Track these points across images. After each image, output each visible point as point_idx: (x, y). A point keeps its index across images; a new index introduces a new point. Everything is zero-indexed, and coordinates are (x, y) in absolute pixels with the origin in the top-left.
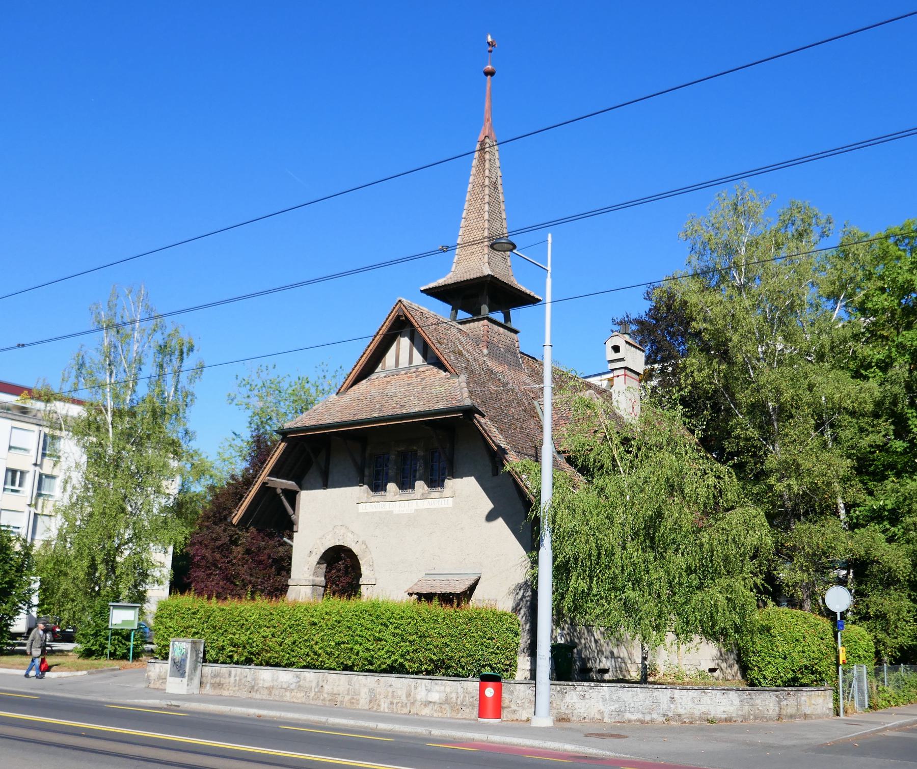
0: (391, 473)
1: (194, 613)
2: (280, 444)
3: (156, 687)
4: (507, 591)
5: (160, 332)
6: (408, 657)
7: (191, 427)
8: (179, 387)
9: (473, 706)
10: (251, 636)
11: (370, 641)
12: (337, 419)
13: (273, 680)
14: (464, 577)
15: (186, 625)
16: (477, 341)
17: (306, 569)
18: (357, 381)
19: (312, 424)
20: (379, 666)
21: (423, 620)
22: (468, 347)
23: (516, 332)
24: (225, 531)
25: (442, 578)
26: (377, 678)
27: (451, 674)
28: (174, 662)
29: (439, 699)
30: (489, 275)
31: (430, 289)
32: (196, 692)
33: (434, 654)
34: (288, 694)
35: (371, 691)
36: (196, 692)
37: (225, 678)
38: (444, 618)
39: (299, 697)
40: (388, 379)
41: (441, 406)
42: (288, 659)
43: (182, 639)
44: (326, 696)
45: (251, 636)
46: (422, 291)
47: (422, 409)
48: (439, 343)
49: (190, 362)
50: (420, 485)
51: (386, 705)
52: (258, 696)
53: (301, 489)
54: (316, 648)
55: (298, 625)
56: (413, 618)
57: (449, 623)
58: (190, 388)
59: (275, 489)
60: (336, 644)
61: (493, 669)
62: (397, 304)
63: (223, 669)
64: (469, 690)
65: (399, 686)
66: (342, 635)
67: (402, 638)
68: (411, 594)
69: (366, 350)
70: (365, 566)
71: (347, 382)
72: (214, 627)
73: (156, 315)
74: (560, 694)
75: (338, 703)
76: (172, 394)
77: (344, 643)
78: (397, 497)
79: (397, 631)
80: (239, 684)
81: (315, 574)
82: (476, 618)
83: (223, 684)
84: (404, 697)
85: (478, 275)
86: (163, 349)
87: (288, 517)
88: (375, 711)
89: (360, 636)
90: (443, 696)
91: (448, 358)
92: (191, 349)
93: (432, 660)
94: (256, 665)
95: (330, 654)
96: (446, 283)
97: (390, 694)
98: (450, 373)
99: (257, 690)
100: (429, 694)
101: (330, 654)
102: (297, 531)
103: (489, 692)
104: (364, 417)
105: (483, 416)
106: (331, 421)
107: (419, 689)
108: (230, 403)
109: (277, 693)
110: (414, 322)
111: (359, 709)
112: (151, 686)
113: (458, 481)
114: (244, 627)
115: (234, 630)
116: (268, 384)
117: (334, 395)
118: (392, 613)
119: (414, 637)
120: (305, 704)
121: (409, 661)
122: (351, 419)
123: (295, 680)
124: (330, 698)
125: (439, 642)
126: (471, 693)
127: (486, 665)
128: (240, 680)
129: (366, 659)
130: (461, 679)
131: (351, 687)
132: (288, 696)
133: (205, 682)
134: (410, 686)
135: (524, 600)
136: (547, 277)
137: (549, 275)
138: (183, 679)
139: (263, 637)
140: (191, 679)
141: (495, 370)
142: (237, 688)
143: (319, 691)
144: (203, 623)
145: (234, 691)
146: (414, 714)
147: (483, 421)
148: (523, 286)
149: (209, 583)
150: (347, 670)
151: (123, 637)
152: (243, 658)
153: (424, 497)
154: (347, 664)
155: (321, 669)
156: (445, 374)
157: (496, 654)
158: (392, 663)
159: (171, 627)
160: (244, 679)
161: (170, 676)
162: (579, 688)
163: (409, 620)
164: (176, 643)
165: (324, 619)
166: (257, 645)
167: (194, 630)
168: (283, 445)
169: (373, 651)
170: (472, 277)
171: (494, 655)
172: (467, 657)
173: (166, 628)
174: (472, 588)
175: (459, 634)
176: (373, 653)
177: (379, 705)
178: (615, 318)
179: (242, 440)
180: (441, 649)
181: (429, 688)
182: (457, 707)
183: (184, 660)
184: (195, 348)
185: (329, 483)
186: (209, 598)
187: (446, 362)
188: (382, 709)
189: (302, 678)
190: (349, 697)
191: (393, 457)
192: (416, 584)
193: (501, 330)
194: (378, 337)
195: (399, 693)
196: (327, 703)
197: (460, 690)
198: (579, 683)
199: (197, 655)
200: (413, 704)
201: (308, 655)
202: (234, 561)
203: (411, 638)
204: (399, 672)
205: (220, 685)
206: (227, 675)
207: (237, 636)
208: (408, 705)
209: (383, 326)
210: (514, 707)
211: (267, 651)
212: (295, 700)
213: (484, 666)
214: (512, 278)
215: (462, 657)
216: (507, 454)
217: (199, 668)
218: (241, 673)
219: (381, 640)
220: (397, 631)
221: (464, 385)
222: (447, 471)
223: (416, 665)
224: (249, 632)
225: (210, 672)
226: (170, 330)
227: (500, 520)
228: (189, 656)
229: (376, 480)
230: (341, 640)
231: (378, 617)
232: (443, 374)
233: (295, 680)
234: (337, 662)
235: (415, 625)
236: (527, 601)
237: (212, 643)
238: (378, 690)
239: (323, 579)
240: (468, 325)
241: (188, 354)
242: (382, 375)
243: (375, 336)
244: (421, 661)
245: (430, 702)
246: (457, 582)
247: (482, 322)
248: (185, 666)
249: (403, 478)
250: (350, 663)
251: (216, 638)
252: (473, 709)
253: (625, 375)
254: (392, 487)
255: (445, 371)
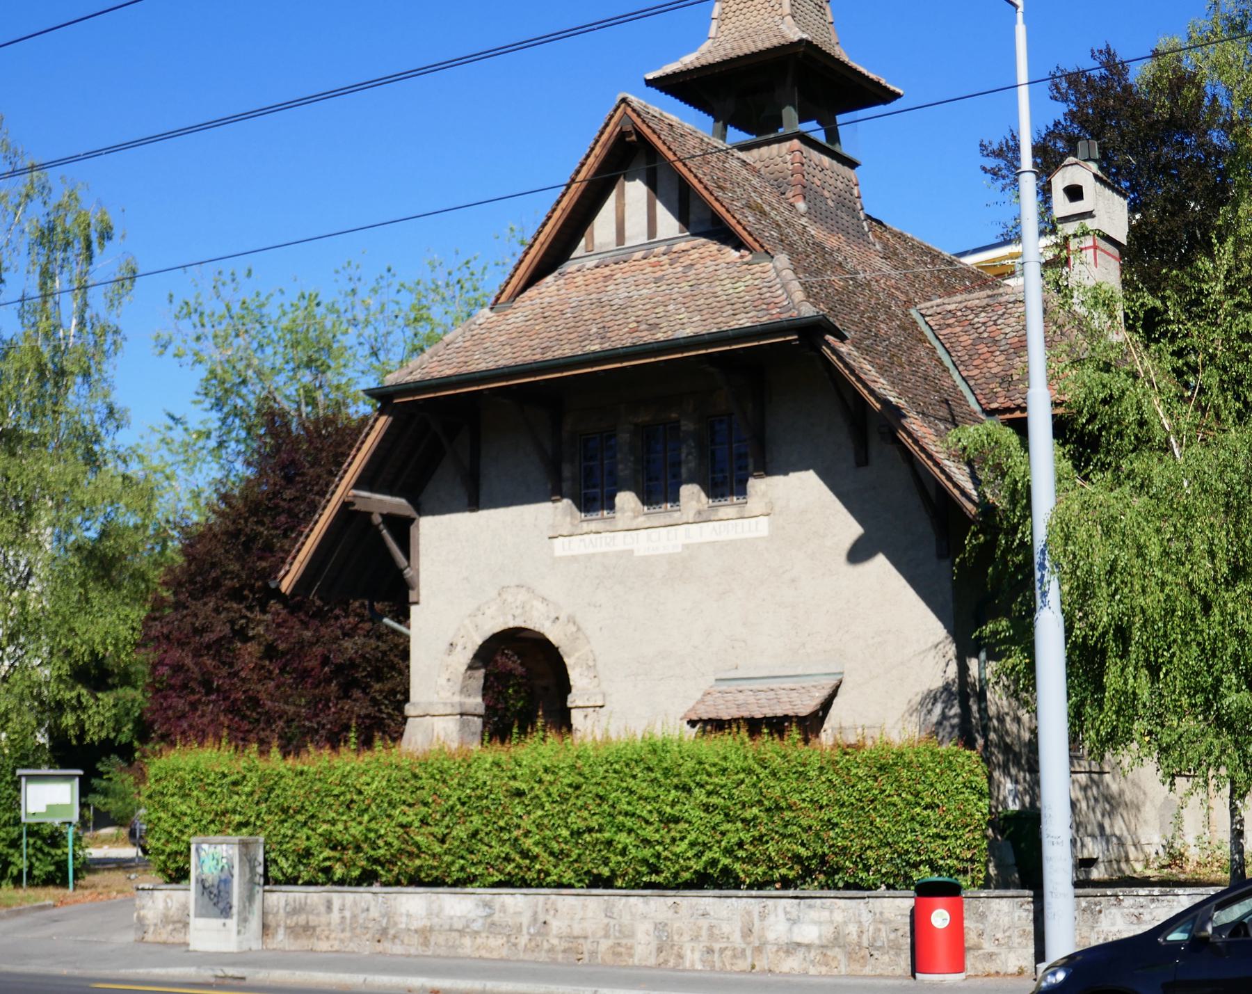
0: (623, 470)
1: (235, 783)
2: (376, 420)
3: (159, 939)
4: (905, 707)
5: (38, 201)
6: (741, 854)
7: (119, 399)
8: (87, 316)
9: (896, 947)
10: (373, 825)
11: (651, 824)
12: (506, 359)
13: (429, 915)
14: (807, 683)
15: (220, 809)
16: (780, 186)
17: (442, 681)
18: (535, 278)
19: (448, 372)
20: (676, 875)
21: (774, 774)
22: (766, 196)
23: (852, 164)
24: (217, 610)
25: (756, 685)
26: (670, 901)
27: (841, 884)
28: (203, 886)
29: (820, 937)
30: (801, 41)
31: (661, 78)
32: (256, 945)
33: (803, 844)
34: (467, 941)
35: (660, 927)
36: (256, 945)
37: (318, 915)
38: (821, 768)
39: (495, 946)
40: (607, 271)
41: (745, 321)
42: (462, 869)
43: (212, 838)
44: (555, 941)
45: (373, 825)
46: (649, 83)
47: (702, 330)
48: (719, 187)
49: (107, 262)
50: (691, 494)
51: (697, 955)
52: (398, 949)
53: (422, 512)
54: (528, 843)
55: (480, 798)
56: (749, 771)
57: (834, 778)
58: (113, 319)
59: (369, 514)
60: (572, 834)
61: (934, 868)
62: (618, 107)
63: (315, 896)
64: (886, 915)
65: (724, 914)
66: (585, 814)
67: (726, 815)
68: (692, 723)
69: (554, 210)
70: (578, 670)
71: (514, 281)
72: (285, 810)
73: (28, 164)
74: (1088, 915)
75: (586, 956)
76: (73, 330)
77: (590, 830)
78: (641, 521)
79: (714, 800)
80: (352, 925)
81: (464, 690)
82: (895, 764)
83: (314, 928)
84: (737, 938)
85: (775, 42)
86: (47, 237)
87: (400, 572)
88: (674, 969)
89: (626, 814)
90: (828, 932)
91: (741, 220)
92: (106, 235)
93: (797, 858)
94: (387, 884)
95: (558, 856)
96: (704, 62)
97: (704, 933)
98: (750, 250)
99: (395, 937)
100: (796, 929)
101: (558, 856)
102: (417, 603)
103: (940, 918)
104: (567, 352)
105: (842, 338)
106: (492, 365)
107: (772, 919)
108: (161, 354)
109: (441, 940)
110: (659, 144)
111: (634, 967)
112: (149, 937)
113: (777, 481)
114: (355, 806)
115: (332, 815)
116: (236, 309)
117: (486, 311)
118: (700, 763)
119: (755, 810)
120: (508, 960)
121: (743, 860)
122: (538, 357)
123: (482, 912)
124: (565, 945)
125: (811, 818)
126: (890, 922)
127: (921, 862)
128: (354, 917)
129: (645, 861)
130: (867, 893)
131: (612, 922)
132: (467, 946)
133: (273, 924)
134: (749, 913)
135: (946, 723)
136: (1015, 22)
137: (1020, 16)
138: (228, 921)
139: (401, 826)
140: (244, 920)
141: (828, 245)
142: (348, 934)
143: (539, 933)
144: (258, 803)
145: (342, 941)
146: (763, 972)
147: (844, 348)
148: (863, 66)
149: (197, 721)
150: (597, 887)
151: (44, 839)
152: (356, 873)
153: (702, 518)
154: (600, 875)
155: (540, 886)
156: (737, 254)
157: (945, 838)
158: (705, 868)
159: (185, 814)
160: (364, 915)
161: (196, 916)
162: (1128, 902)
163: (742, 776)
164: (205, 846)
165: (540, 781)
166: (387, 844)
167: (238, 818)
168: (383, 422)
169: (659, 843)
170: (761, 46)
171: (940, 842)
172: (879, 848)
173: (173, 815)
174: (827, 705)
175: (861, 801)
176: (659, 848)
177: (680, 956)
178: (986, 143)
179: (186, 430)
180: (817, 835)
181: (794, 915)
182: (861, 952)
183: (226, 882)
184: (117, 232)
185: (482, 499)
186: (263, 753)
187: (739, 228)
188: (687, 965)
189: (497, 907)
190: (610, 942)
191: (624, 437)
192: (701, 701)
193: (826, 160)
194: (574, 186)
195: (726, 928)
196: (560, 957)
197: (866, 918)
198: (1127, 890)
199: (252, 869)
200: (759, 950)
201: (507, 859)
202: (243, 674)
203: (748, 814)
204: (720, 887)
205: (308, 929)
206: (322, 909)
207: (340, 826)
208: (748, 953)
209: (588, 156)
210: (988, 946)
211: (411, 855)
212: (484, 953)
213: (916, 866)
214: (837, 48)
215: (870, 847)
216: (905, 416)
217: (258, 897)
218: (355, 903)
219: (677, 820)
220: (714, 800)
221: (788, 274)
222: (751, 461)
223: (760, 870)
224: (366, 818)
225: (282, 903)
226: (59, 195)
227: (881, 562)
228: (236, 871)
229: (587, 487)
230: (582, 825)
231: (666, 772)
232: (733, 254)
233: (482, 912)
234: (575, 871)
235: (754, 785)
236: (953, 727)
237: (281, 843)
238: (676, 925)
239: (479, 700)
240: (755, 152)
241: (101, 245)
242: (591, 263)
243: (568, 186)
244: (770, 859)
245: (799, 945)
246: (794, 694)
247: (787, 144)
248: (229, 893)
249: (650, 479)
250: (606, 872)
251: (290, 833)
252: (897, 955)
253: (1095, 247)
254: (626, 500)
255: (737, 248)
